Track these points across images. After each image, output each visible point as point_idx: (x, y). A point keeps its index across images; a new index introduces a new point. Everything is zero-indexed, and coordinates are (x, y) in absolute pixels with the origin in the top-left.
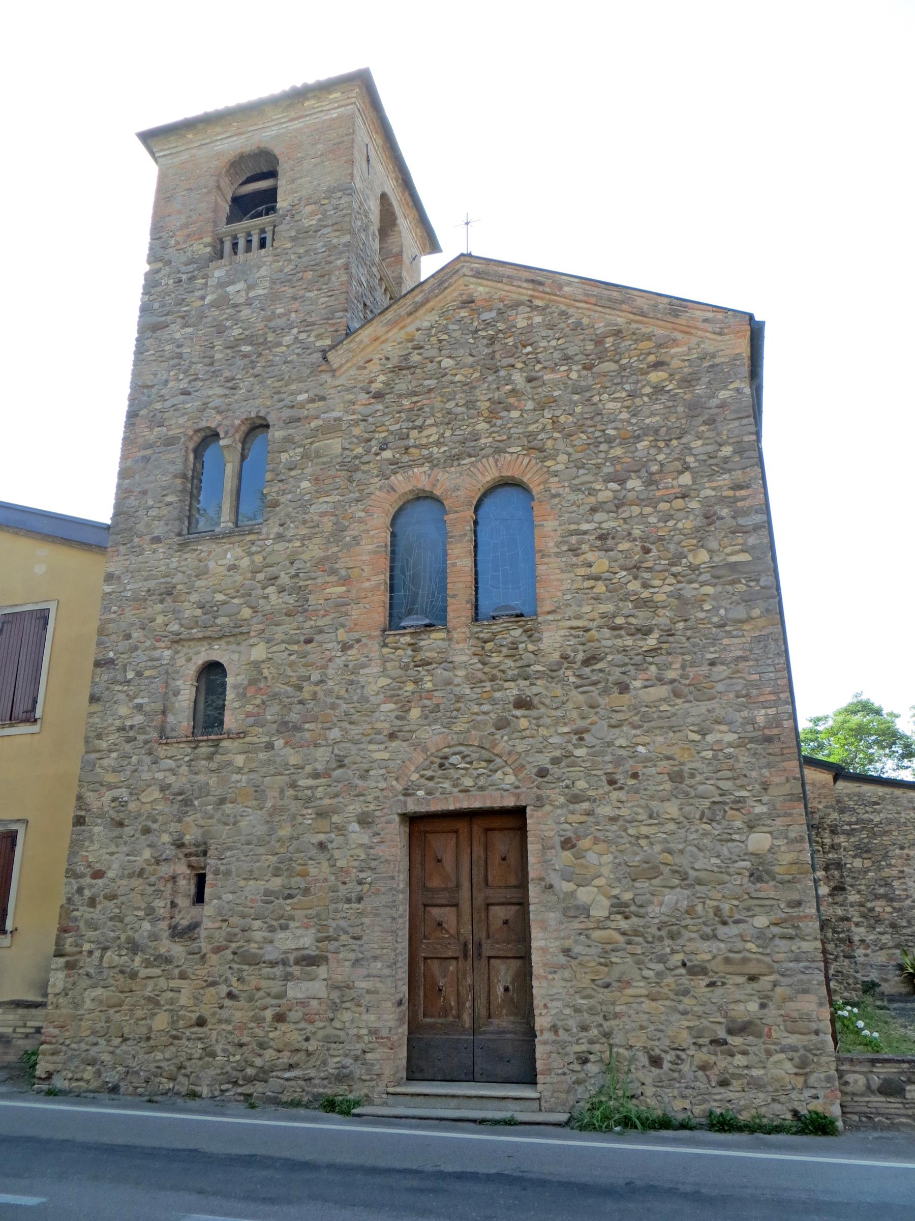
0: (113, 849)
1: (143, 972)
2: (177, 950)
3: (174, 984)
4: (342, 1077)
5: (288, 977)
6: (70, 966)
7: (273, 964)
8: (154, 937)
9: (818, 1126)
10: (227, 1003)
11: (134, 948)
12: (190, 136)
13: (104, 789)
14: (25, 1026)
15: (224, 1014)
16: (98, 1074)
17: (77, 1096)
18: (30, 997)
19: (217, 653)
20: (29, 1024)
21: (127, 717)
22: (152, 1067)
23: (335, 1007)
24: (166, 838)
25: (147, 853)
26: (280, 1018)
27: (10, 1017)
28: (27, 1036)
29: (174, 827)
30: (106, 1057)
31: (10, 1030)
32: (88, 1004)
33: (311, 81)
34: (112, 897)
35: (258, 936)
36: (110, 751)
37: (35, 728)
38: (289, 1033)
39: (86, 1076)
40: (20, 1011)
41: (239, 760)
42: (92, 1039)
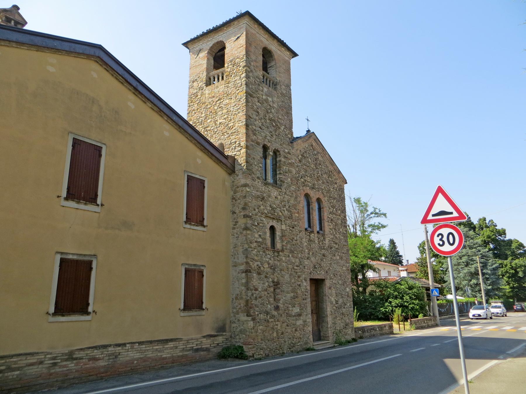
0: (259, 282)
1: (270, 320)
2: (275, 313)
3: (277, 323)
4: (306, 343)
5: (297, 320)
6: (253, 319)
7: (294, 316)
8: (271, 310)
9: (354, 340)
10: (287, 327)
11: (267, 313)
12: (256, 26)
13: (254, 261)
14: (214, 344)
15: (286, 331)
16: (264, 352)
17: (260, 359)
18: (213, 333)
19: (274, 223)
20: (215, 342)
21: (256, 238)
22: (274, 347)
23: (304, 326)
24: (271, 280)
25: (267, 284)
26: (296, 330)
27: (209, 341)
28: (215, 347)
29: (272, 276)
30: (265, 347)
31: (209, 346)
32: (259, 331)
33: (275, 33)
34: (260, 297)
35: (291, 309)
36: (255, 249)
37: (205, 229)
38: (297, 334)
39: (262, 353)
40: (212, 339)
41: (284, 258)
42: (261, 342)
